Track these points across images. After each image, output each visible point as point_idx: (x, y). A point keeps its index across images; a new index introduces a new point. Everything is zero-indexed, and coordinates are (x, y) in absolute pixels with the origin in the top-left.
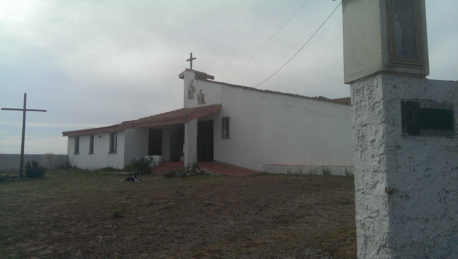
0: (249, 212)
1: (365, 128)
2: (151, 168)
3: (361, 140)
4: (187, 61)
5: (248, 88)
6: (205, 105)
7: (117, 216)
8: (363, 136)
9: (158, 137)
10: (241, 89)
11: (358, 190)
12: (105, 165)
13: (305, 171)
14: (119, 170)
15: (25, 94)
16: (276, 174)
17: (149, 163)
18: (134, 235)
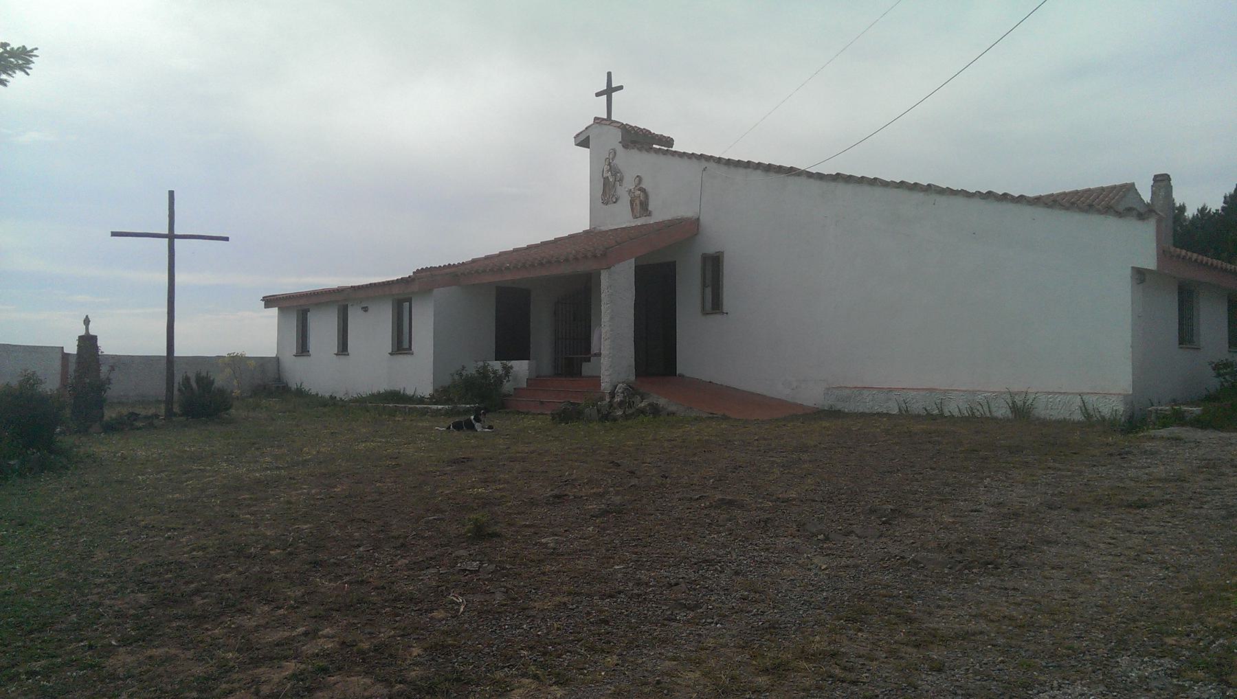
0: (857, 529)
2: (505, 396)
6: (651, 221)
7: (480, 534)
9: (523, 309)
10: (759, 172)
12: (382, 387)
14: (421, 400)
15: (171, 194)
17: (499, 380)
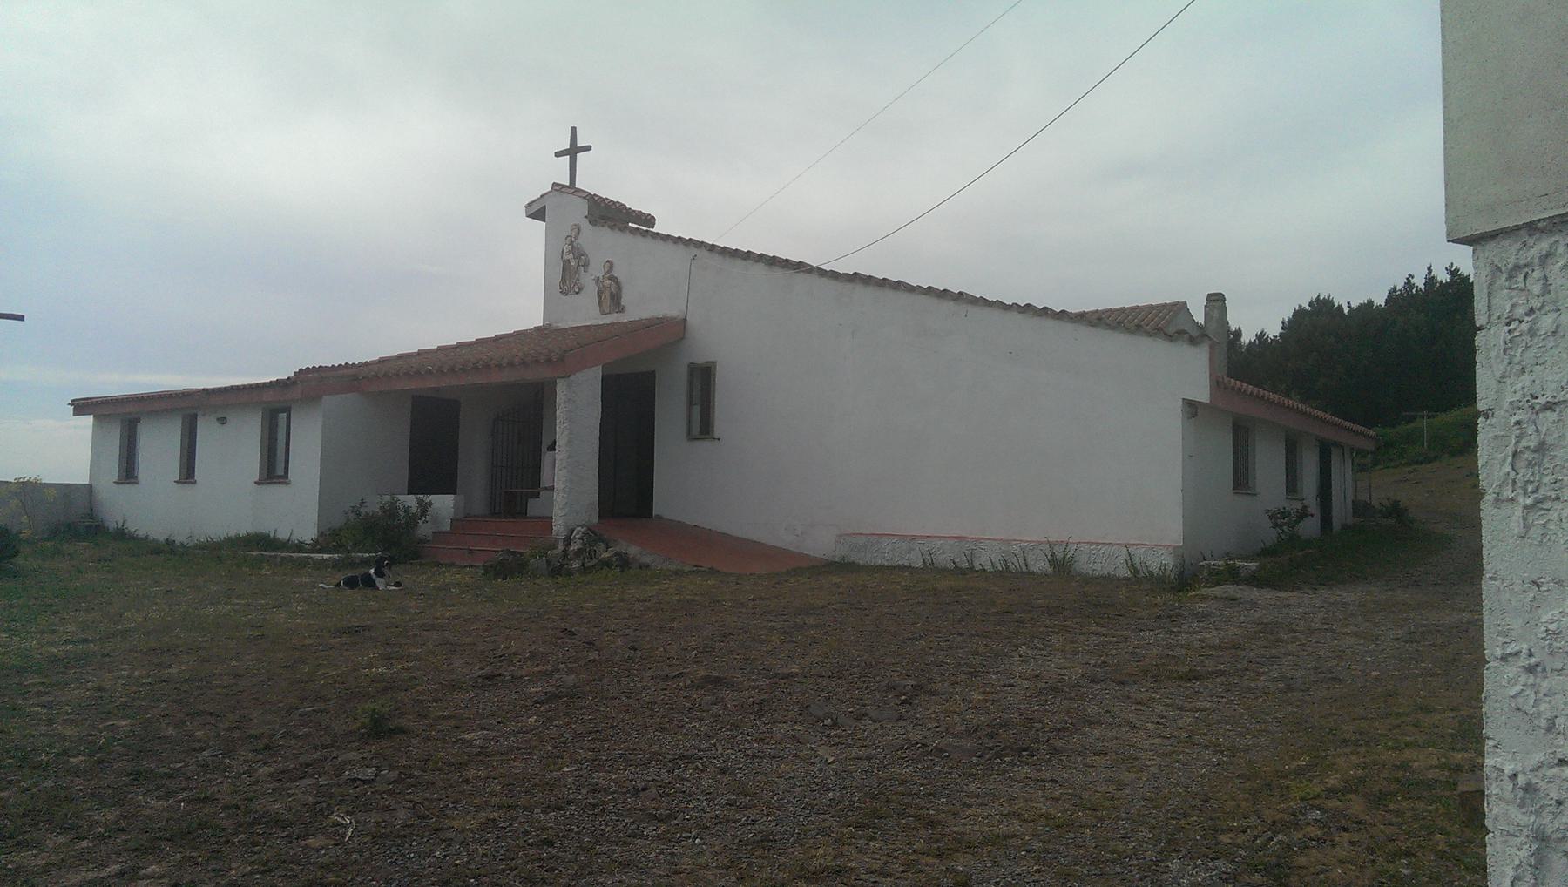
1: (1551, 416)
2: (421, 541)
3: (1530, 464)
4: (558, 154)
5: (786, 264)
6: (624, 318)
7: (378, 729)
8: (1541, 448)
9: (450, 424)
10: (761, 265)
11: (1504, 658)
13: (987, 559)
14: (299, 547)
16: (881, 567)
17: (412, 520)
18: (479, 808)
